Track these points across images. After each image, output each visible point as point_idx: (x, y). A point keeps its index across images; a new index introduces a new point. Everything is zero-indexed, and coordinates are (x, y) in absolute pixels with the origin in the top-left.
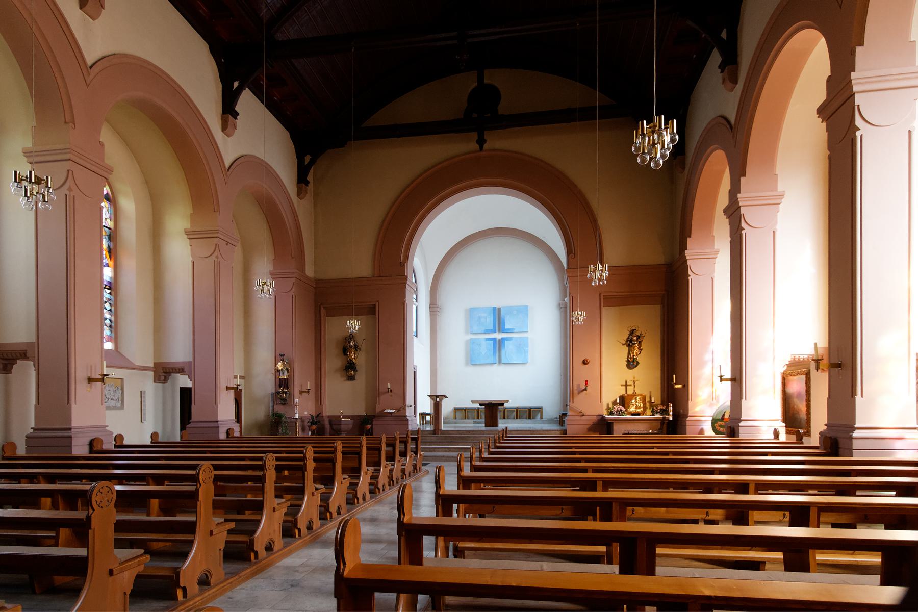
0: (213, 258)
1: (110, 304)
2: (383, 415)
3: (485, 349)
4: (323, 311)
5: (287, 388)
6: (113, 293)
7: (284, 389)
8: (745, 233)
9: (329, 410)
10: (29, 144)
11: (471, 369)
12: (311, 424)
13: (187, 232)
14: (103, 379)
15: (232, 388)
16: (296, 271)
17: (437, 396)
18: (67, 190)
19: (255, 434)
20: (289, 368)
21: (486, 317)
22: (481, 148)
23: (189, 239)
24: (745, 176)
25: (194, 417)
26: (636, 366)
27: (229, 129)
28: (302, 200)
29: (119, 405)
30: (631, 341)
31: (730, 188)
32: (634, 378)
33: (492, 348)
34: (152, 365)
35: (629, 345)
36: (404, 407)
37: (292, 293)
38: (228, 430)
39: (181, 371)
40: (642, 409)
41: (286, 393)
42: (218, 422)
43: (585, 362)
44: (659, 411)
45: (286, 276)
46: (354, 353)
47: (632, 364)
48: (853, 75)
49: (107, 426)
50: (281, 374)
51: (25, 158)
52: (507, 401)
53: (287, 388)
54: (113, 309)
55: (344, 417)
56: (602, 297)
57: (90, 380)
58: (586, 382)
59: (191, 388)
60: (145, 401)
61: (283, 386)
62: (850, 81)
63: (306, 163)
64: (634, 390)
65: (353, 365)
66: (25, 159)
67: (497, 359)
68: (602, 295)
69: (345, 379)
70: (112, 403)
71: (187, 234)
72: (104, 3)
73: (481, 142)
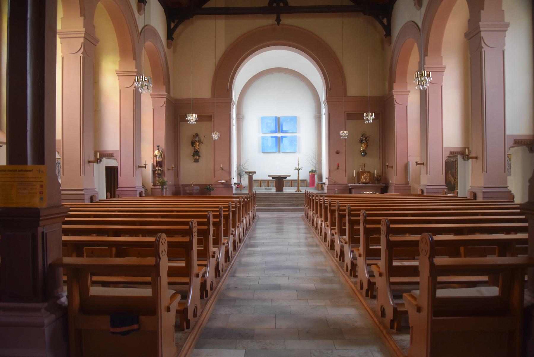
3: (271, 143)
13: (117, 72)
17: (250, 172)
18: (81, 54)
22: (278, 24)
23: (118, 76)
24: (427, 56)
31: (419, 61)
36: (230, 180)
45: (156, 97)
48: (481, 23)
49: (95, 189)
52: (289, 176)
56: (346, 114)
62: (479, 26)
65: (198, 152)
67: (278, 150)
68: (346, 113)
71: (117, 73)
73: (278, 20)
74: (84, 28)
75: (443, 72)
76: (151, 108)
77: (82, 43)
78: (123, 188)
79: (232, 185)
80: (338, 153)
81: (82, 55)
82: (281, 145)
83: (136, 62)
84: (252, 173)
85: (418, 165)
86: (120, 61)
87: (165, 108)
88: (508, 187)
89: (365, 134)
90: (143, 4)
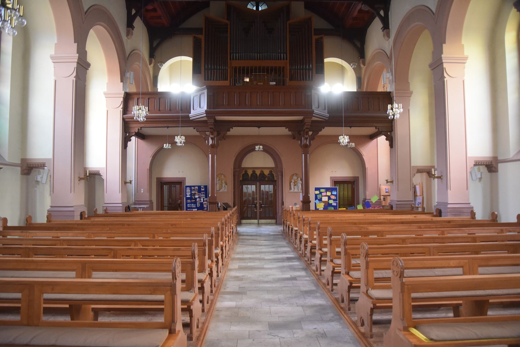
8: (447, 80)
10: (105, 90)
23: (54, 63)
27: (129, 36)
38: (81, 213)
48: (443, 56)
51: (51, 60)
62: (441, 58)
63: (133, 14)
66: (51, 60)
74: (77, 53)
75: (465, 63)
77: (75, 68)
78: (55, 208)
81: (74, 79)
83: (123, 84)
85: (388, 183)
86: (108, 83)
87: (122, 110)
88: (470, 203)
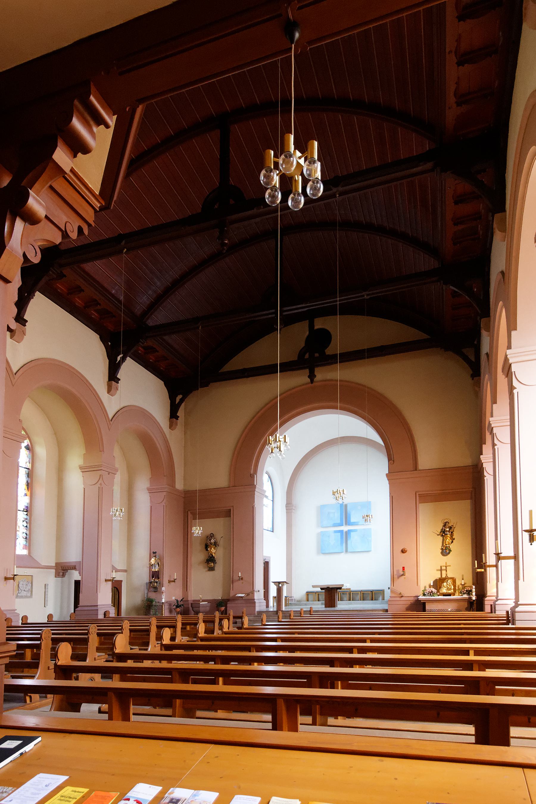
0: (98, 485)
1: (27, 522)
2: (235, 599)
3: (334, 540)
4: (190, 515)
5: (159, 578)
6: (29, 514)
7: (156, 579)
9: (193, 595)
11: (322, 557)
12: (176, 607)
14: (14, 577)
15: (109, 580)
16: (166, 486)
17: (279, 583)
19: (134, 616)
20: (160, 563)
21: (335, 512)
22: (312, 381)
25: (81, 603)
26: (449, 553)
28: (174, 431)
29: (29, 595)
30: (444, 532)
32: (446, 563)
33: (340, 540)
34: (54, 565)
35: (442, 535)
36: (253, 592)
37: (163, 504)
39: (74, 568)
40: (452, 590)
41: (157, 583)
42: (97, 606)
43: (403, 551)
44: (465, 592)
46: (214, 548)
47: (445, 551)
49: (16, 610)
50: (153, 568)
53: (159, 578)
54: (28, 526)
55: (203, 601)
57: (6, 579)
58: (403, 568)
59: (80, 580)
60: (47, 591)
61: (155, 576)
64: (446, 575)
68: (417, 494)
69: (207, 570)
70: (24, 594)
72: (25, 333)
73: (312, 376)
76: (148, 505)
79: (255, 599)
80: (404, 551)
82: (349, 542)
84: (282, 583)
89: (212, 533)
90: (113, 382)
